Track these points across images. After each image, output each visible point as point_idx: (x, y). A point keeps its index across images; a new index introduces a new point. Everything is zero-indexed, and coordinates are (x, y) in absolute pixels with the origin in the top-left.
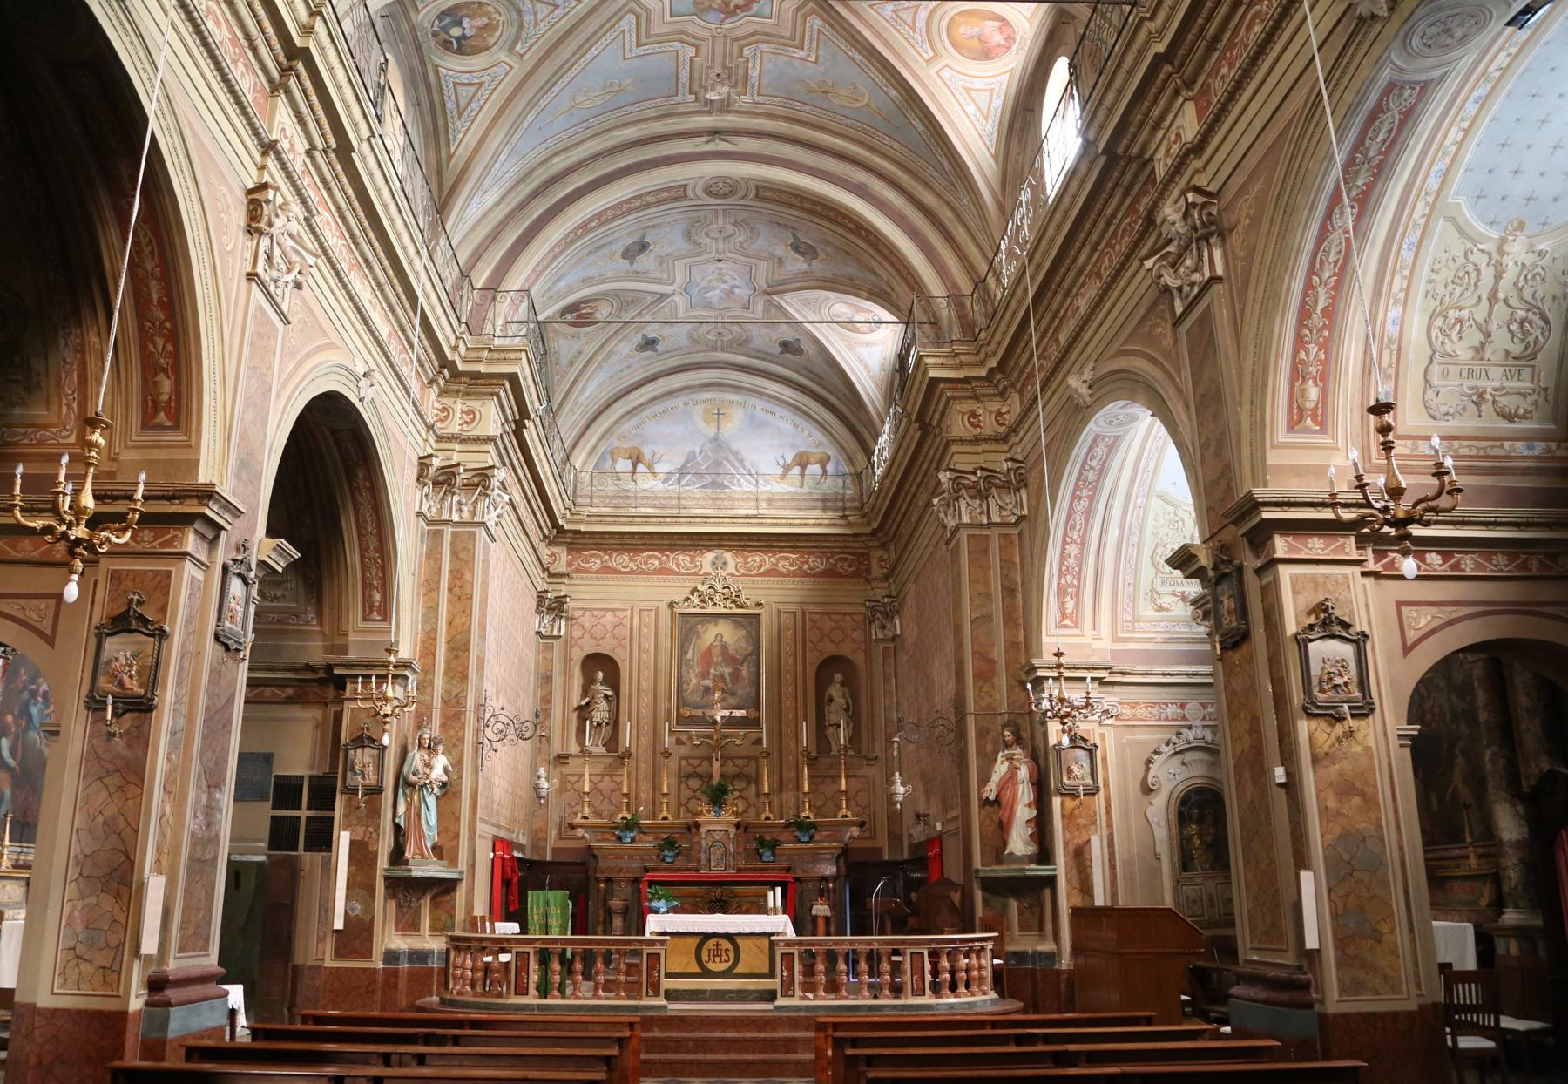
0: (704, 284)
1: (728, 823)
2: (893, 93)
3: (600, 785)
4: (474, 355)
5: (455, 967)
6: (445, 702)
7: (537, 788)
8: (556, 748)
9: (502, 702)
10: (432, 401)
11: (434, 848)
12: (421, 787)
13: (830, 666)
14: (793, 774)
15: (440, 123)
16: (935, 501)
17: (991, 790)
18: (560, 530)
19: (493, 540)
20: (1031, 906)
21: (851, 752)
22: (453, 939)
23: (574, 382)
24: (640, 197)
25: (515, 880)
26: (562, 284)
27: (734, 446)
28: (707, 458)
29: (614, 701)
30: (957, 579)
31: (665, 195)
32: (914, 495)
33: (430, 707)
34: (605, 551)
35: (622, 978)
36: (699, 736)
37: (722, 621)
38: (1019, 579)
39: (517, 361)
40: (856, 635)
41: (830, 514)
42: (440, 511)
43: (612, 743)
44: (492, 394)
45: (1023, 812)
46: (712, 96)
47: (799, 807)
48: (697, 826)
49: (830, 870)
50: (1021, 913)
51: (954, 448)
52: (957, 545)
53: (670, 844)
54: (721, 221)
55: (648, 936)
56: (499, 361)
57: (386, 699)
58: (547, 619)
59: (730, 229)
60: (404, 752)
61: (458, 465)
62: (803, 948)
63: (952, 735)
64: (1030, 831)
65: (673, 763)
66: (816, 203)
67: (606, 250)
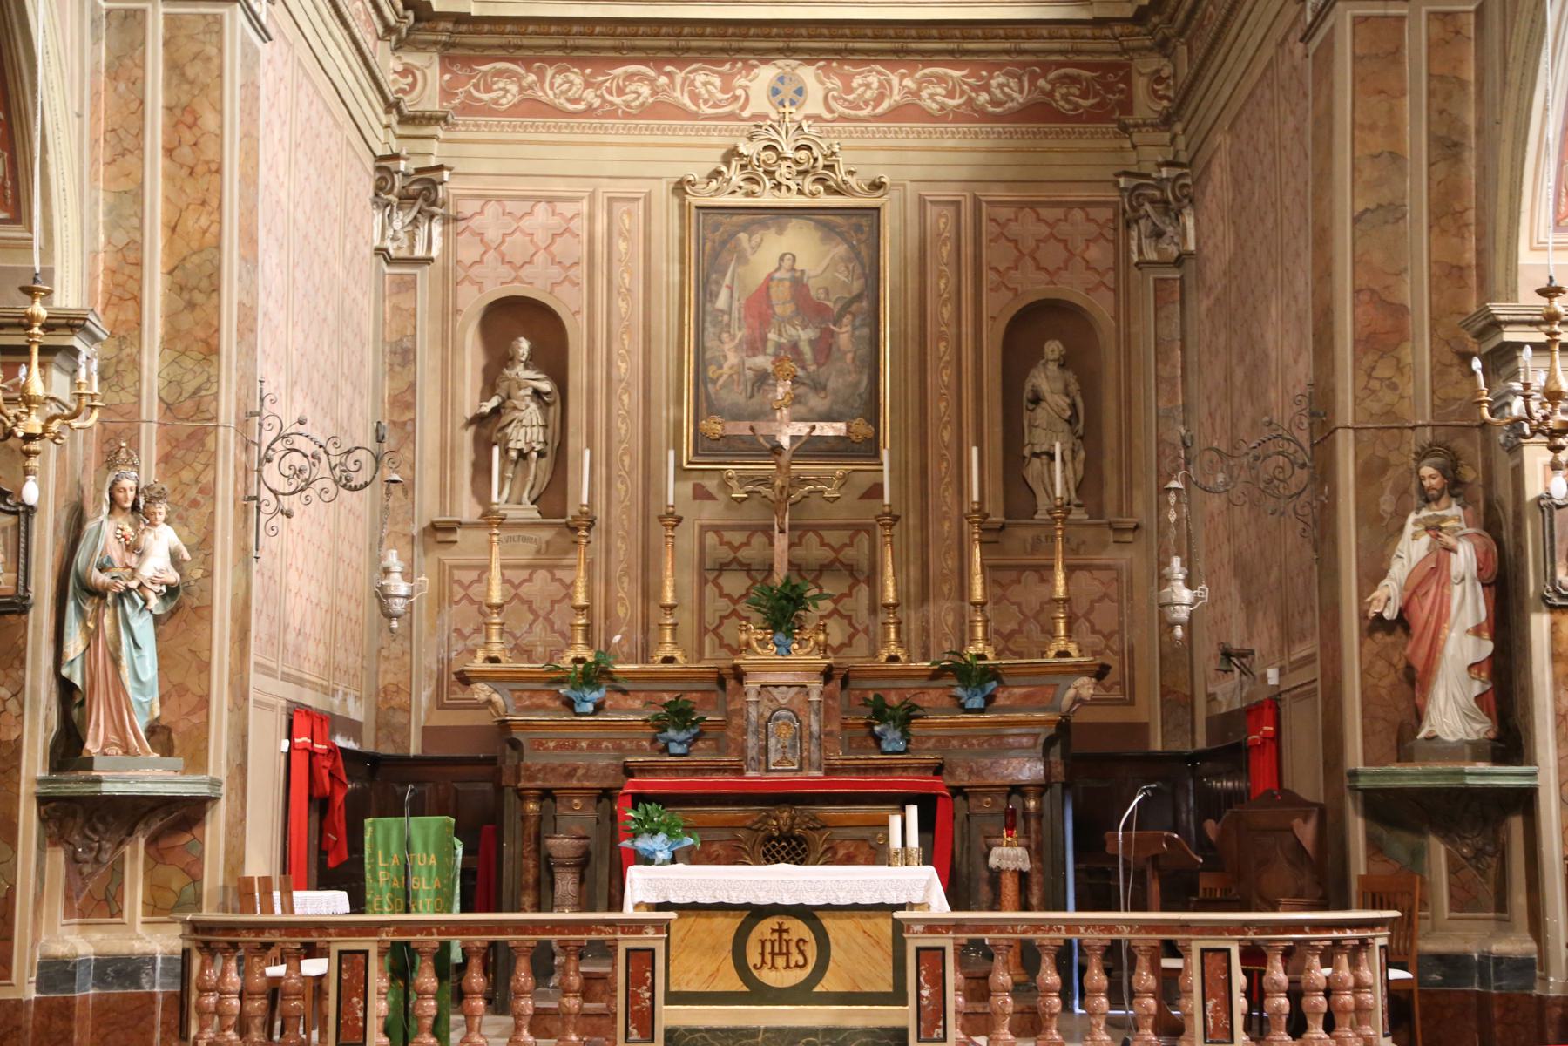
1: (807, 669)
3: (525, 590)
5: (203, 990)
6: (168, 407)
7: (382, 595)
8: (428, 508)
9: (301, 406)
11: (152, 730)
12: (120, 597)
13: (1035, 324)
14: (951, 563)
17: (1388, 597)
19: (266, 36)
20: (1479, 853)
21: (1078, 515)
22: (196, 927)
25: (339, 799)
29: (556, 402)
30: (1325, 120)
33: (133, 419)
34: (527, 63)
35: (573, 1003)
36: (743, 480)
37: (794, 222)
38: (1471, 119)
40: (1094, 253)
43: (552, 496)
45: (1462, 646)
48: (739, 675)
49: (1028, 770)
50: (1454, 869)
52: (1328, 43)
53: (679, 714)
55: (629, 912)
57: (28, 401)
58: (400, 220)
60: (77, 521)
62: (964, 937)
63: (1303, 475)
64: (1477, 687)
65: (687, 539)
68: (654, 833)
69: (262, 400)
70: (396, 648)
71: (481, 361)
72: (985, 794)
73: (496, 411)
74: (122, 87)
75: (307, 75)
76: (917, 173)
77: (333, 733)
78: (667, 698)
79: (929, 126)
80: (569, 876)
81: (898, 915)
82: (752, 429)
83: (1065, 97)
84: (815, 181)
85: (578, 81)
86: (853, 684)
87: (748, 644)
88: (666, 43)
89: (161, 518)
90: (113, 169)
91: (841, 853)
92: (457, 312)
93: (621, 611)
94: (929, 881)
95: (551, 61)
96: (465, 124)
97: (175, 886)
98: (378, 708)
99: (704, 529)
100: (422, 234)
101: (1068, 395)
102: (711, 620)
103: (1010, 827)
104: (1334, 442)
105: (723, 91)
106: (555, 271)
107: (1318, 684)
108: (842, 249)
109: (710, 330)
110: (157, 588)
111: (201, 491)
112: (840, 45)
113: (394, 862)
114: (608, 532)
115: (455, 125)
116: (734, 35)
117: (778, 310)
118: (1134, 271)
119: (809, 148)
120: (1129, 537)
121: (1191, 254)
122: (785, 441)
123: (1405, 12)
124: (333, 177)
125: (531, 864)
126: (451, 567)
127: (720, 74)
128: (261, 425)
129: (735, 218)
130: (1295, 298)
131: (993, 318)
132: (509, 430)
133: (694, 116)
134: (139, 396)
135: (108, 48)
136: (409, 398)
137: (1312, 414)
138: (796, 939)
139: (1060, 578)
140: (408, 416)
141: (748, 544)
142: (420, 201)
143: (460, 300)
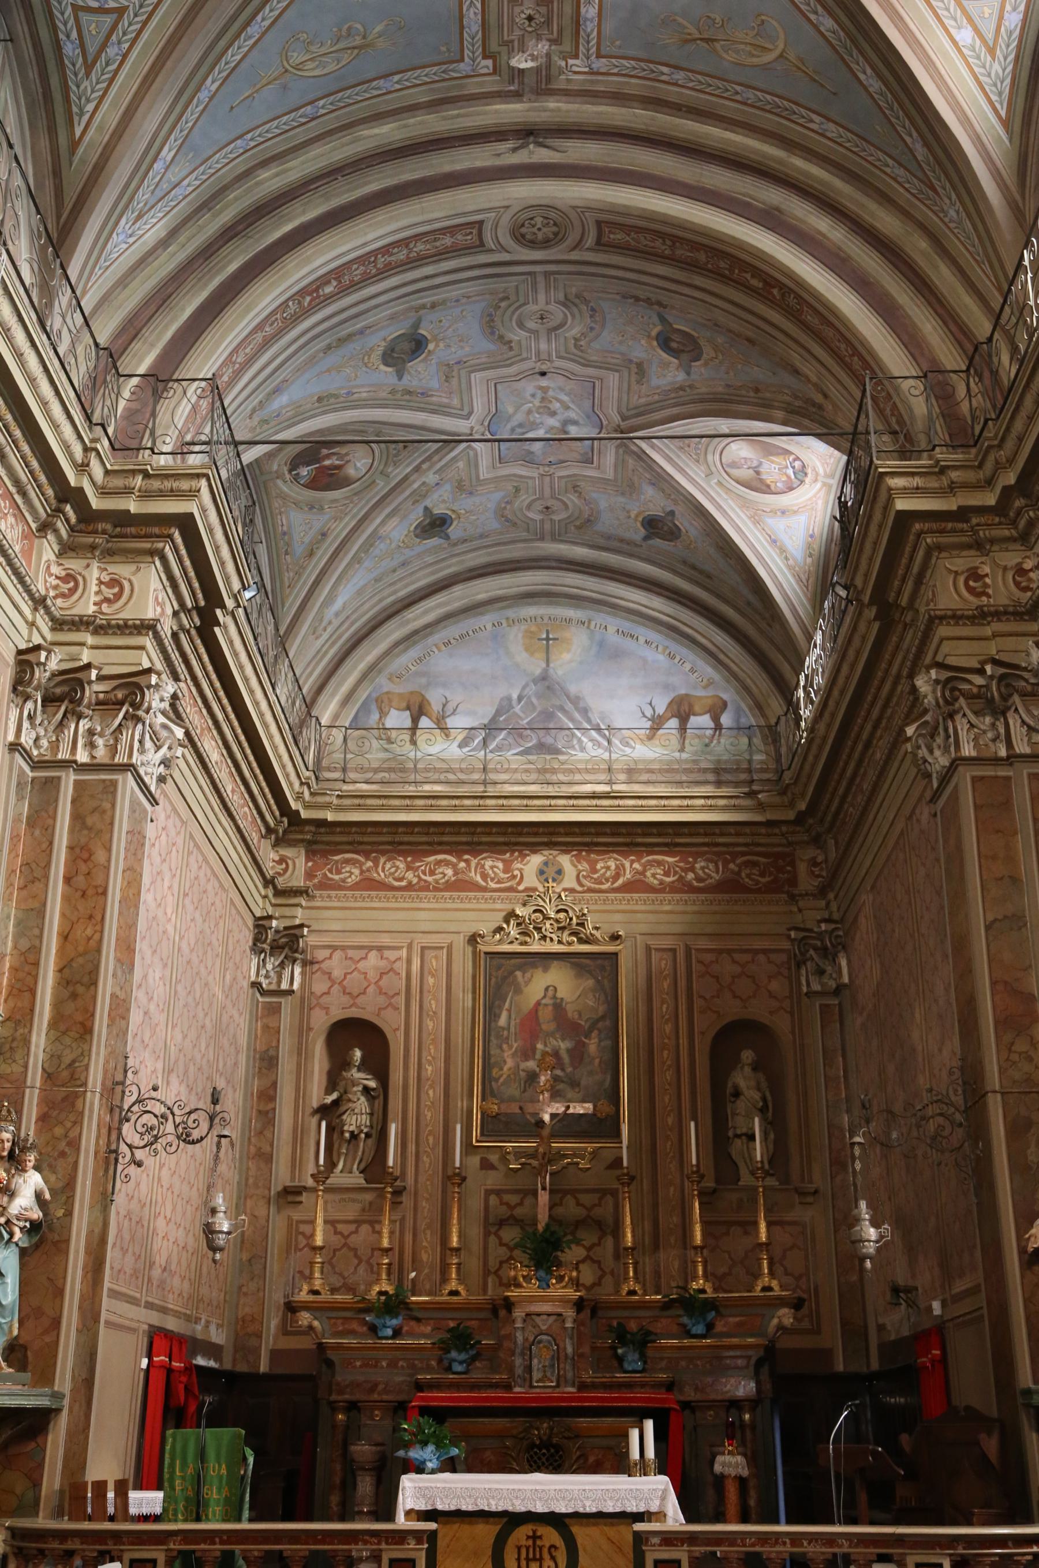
0: (519, 417)
1: (563, 1300)
2: (827, 23)
3: (353, 1240)
4: (118, 482)
6: (49, 1076)
7: (209, 1230)
8: (282, 1176)
10: (45, 562)
13: (733, 1038)
15: (55, 82)
16: (910, 731)
18: (293, 817)
19: (154, 801)
23: (317, 583)
24: (404, 243)
26: (283, 400)
27: (573, 689)
29: (379, 1097)
31: (448, 241)
32: (868, 745)
34: (367, 855)
36: (518, 1153)
39: (193, 494)
40: (774, 986)
42: (55, 746)
44: (152, 553)
46: (522, 62)
47: (689, 1275)
48: (509, 1305)
49: (744, 1388)
51: (943, 631)
52: (955, 797)
53: (460, 1339)
54: (542, 297)
55: (401, 1521)
56: (162, 494)
59: (557, 312)
61: (88, 666)
62: (699, 1550)
63: (960, 1132)
65: (475, 1203)
66: (695, 246)
67: (354, 346)
68: (424, 1444)
69: (126, 1072)
70: (253, 1286)
71: (326, 1066)
72: (709, 1408)
73: (336, 1103)
74: (37, 832)
75: (196, 845)
76: (644, 928)
77: (194, 1355)
78: (452, 1324)
79: (652, 896)
80: (368, 1479)
81: (639, 1527)
82: (521, 1108)
83: (748, 876)
84: (571, 934)
85: (402, 866)
86: (600, 1313)
87: (515, 1278)
88: (464, 839)
89: (30, 1164)
90: (25, 892)
91: (591, 1459)
92: (310, 1029)
93: (424, 1257)
94: (665, 1491)
95: (383, 853)
96: (321, 896)
97: (18, 1490)
98: (237, 1334)
99: (488, 1193)
100: (287, 973)
101: (759, 1089)
102: (493, 1264)
103: (731, 1438)
104: (985, 1106)
105: (505, 871)
106: (382, 1000)
107: (985, 1311)
108: (590, 982)
109: (494, 1041)
110: (22, 1224)
111: (69, 1144)
112: (587, 840)
113: (190, 1471)
114: (416, 1194)
115: (314, 897)
116: (512, 833)
117: (544, 1027)
118: (805, 999)
119: (566, 911)
120: (810, 1199)
121: (845, 985)
122: (547, 1118)
123: (1011, 774)
124: (216, 925)
125: (338, 1467)
126: (299, 1222)
127: (503, 861)
128: (123, 1092)
129: (513, 961)
130: (936, 1001)
131: (703, 1033)
132: (344, 1117)
133: (485, 889)
134: (26, 1067)
135: (30, 804)
136: (272, 1093)
137: (964, 1083)
138: (548, 1545)
139: (763, 1227)
140: (270, 1106)
141: (521, 1204)
142: (286, 950)
143: (312, 1021)
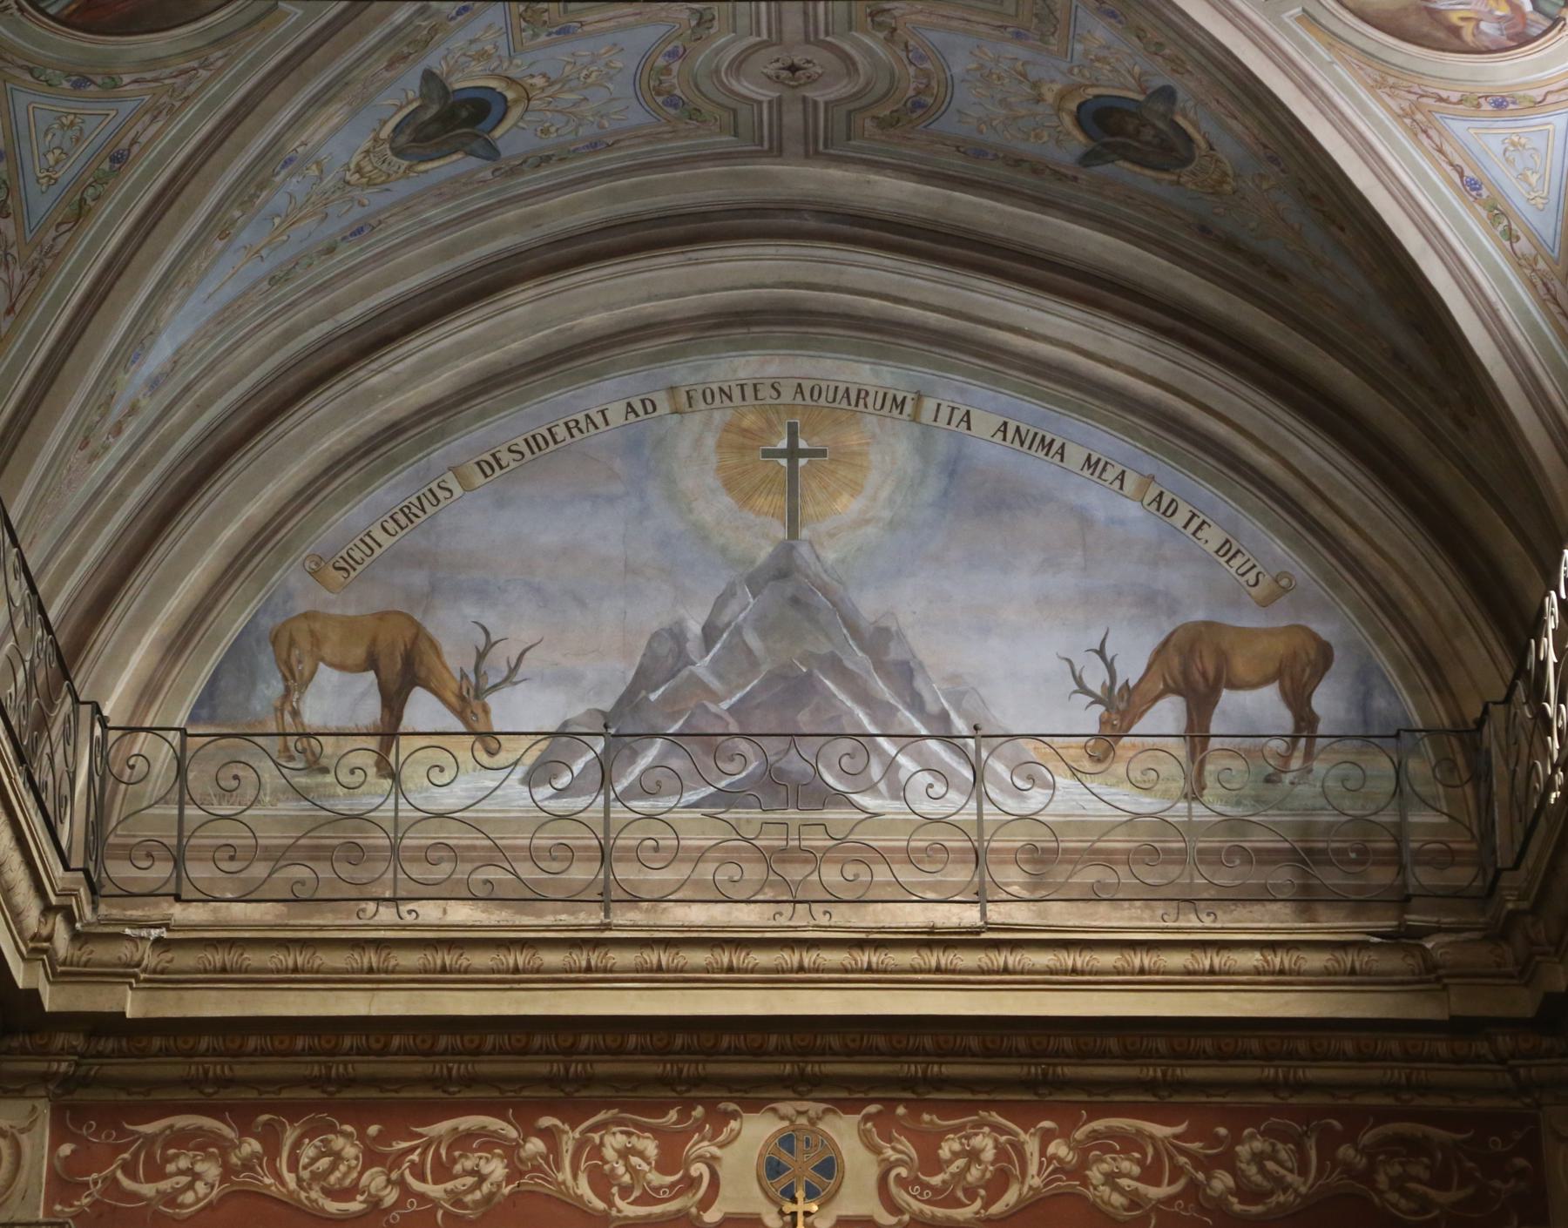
27: (868, 606)
28: (739, 659)
34: (243, 1118)
41: (1332, 924)
